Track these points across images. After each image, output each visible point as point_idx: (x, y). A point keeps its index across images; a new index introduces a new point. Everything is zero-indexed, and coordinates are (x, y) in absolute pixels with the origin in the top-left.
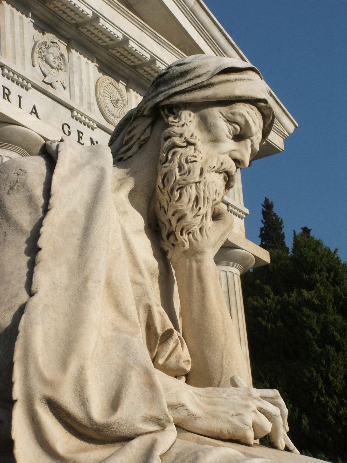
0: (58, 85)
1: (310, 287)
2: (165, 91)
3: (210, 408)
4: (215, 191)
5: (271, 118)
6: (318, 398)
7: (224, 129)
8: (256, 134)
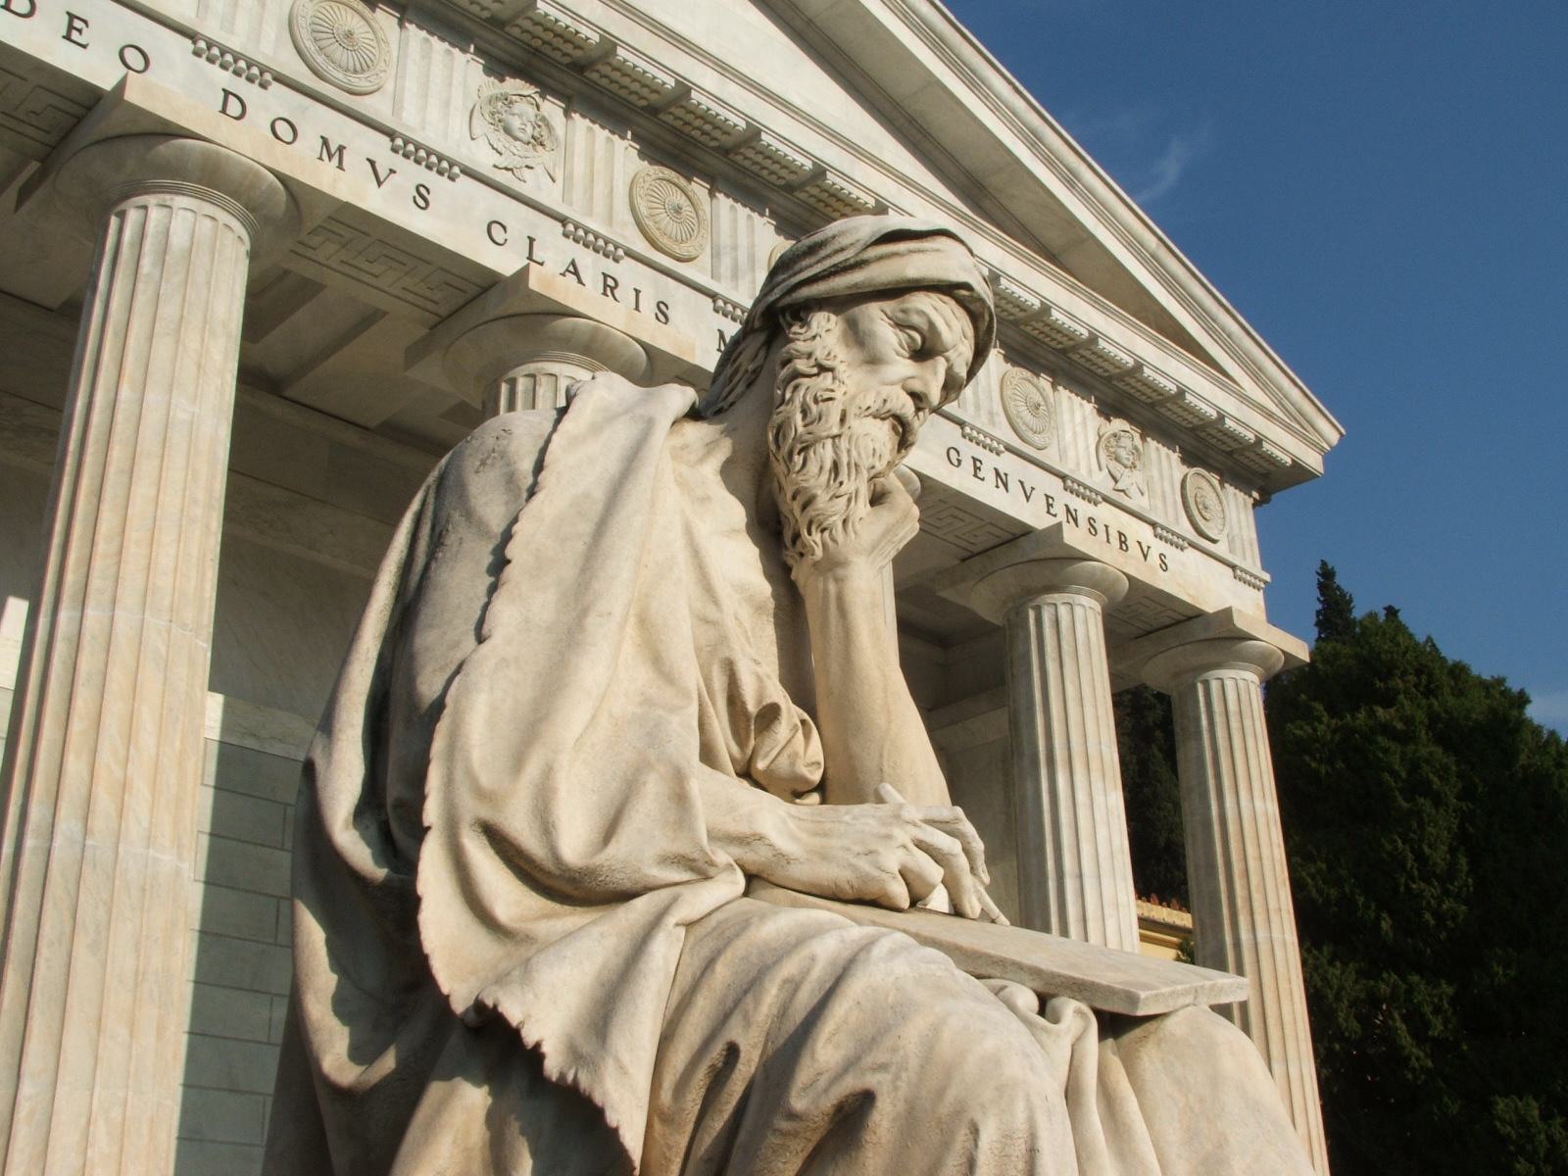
1: (1388, 701)
2: (784, 280)
3: (817, 841)
4: (872, 452)
5: (987, 318)
6: (1407, 886)
7: (888, 338)
8: (954, 346)
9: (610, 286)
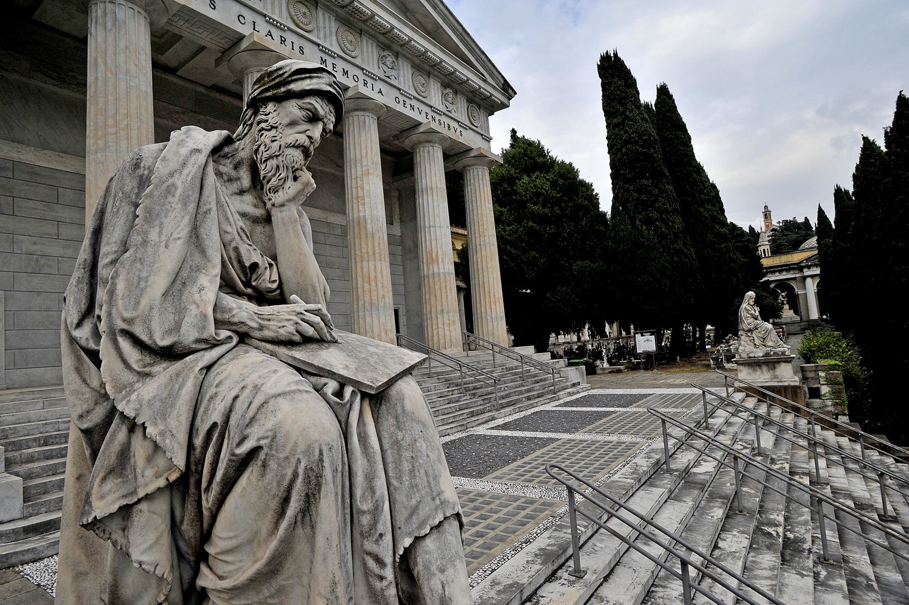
0: (393, 78)
9: (283, 41)
